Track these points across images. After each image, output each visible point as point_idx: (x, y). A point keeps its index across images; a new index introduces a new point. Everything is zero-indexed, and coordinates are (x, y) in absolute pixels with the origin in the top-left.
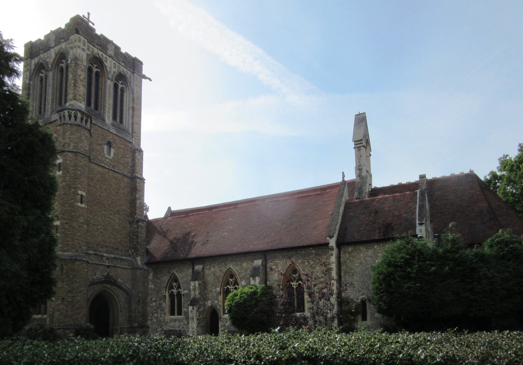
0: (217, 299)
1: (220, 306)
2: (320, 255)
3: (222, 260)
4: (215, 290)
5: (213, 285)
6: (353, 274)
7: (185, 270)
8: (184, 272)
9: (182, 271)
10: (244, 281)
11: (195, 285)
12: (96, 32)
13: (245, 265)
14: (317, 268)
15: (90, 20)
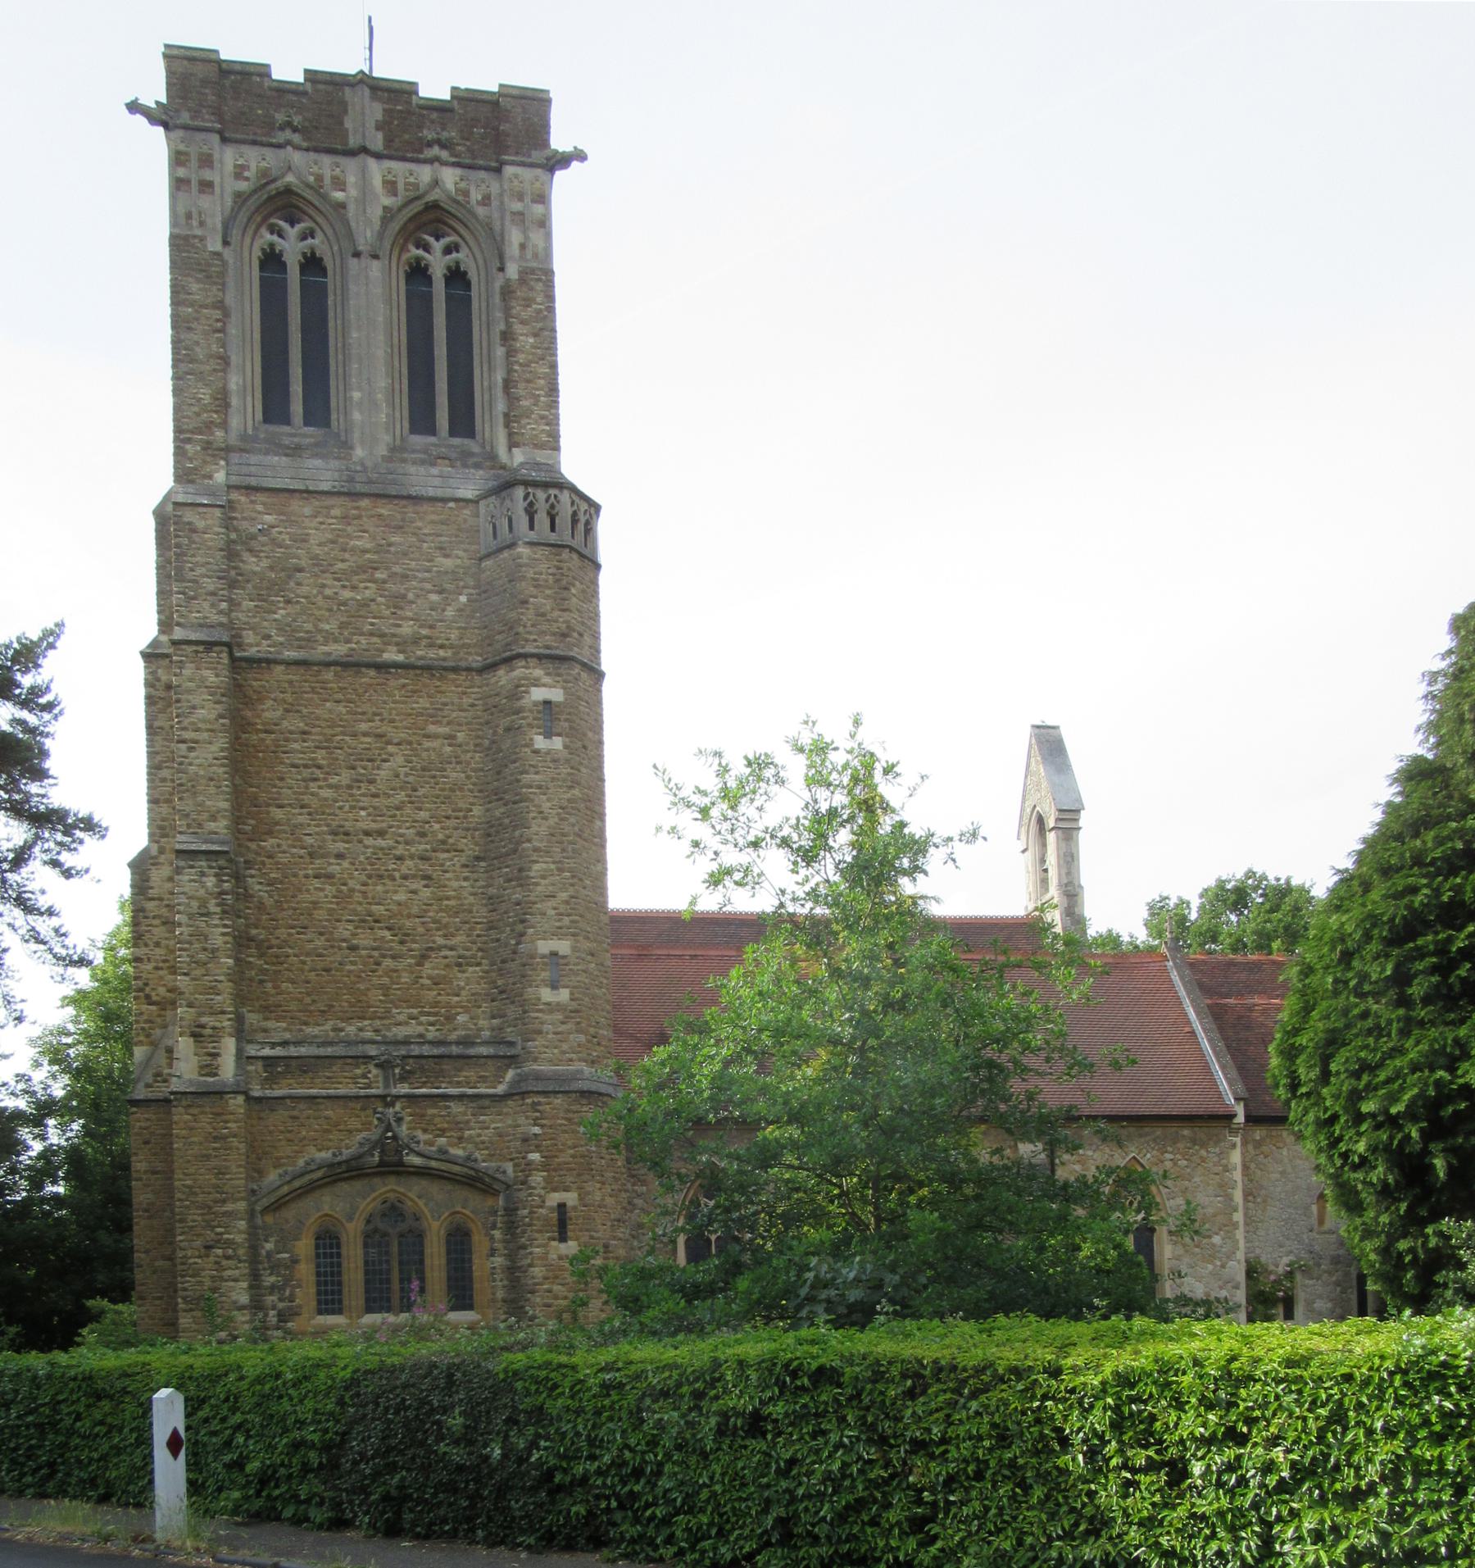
2: (1203, 1145)
6: (1265, 1201)
12: (422, 94)
14: (1197, 1179)
15: (161, 129)
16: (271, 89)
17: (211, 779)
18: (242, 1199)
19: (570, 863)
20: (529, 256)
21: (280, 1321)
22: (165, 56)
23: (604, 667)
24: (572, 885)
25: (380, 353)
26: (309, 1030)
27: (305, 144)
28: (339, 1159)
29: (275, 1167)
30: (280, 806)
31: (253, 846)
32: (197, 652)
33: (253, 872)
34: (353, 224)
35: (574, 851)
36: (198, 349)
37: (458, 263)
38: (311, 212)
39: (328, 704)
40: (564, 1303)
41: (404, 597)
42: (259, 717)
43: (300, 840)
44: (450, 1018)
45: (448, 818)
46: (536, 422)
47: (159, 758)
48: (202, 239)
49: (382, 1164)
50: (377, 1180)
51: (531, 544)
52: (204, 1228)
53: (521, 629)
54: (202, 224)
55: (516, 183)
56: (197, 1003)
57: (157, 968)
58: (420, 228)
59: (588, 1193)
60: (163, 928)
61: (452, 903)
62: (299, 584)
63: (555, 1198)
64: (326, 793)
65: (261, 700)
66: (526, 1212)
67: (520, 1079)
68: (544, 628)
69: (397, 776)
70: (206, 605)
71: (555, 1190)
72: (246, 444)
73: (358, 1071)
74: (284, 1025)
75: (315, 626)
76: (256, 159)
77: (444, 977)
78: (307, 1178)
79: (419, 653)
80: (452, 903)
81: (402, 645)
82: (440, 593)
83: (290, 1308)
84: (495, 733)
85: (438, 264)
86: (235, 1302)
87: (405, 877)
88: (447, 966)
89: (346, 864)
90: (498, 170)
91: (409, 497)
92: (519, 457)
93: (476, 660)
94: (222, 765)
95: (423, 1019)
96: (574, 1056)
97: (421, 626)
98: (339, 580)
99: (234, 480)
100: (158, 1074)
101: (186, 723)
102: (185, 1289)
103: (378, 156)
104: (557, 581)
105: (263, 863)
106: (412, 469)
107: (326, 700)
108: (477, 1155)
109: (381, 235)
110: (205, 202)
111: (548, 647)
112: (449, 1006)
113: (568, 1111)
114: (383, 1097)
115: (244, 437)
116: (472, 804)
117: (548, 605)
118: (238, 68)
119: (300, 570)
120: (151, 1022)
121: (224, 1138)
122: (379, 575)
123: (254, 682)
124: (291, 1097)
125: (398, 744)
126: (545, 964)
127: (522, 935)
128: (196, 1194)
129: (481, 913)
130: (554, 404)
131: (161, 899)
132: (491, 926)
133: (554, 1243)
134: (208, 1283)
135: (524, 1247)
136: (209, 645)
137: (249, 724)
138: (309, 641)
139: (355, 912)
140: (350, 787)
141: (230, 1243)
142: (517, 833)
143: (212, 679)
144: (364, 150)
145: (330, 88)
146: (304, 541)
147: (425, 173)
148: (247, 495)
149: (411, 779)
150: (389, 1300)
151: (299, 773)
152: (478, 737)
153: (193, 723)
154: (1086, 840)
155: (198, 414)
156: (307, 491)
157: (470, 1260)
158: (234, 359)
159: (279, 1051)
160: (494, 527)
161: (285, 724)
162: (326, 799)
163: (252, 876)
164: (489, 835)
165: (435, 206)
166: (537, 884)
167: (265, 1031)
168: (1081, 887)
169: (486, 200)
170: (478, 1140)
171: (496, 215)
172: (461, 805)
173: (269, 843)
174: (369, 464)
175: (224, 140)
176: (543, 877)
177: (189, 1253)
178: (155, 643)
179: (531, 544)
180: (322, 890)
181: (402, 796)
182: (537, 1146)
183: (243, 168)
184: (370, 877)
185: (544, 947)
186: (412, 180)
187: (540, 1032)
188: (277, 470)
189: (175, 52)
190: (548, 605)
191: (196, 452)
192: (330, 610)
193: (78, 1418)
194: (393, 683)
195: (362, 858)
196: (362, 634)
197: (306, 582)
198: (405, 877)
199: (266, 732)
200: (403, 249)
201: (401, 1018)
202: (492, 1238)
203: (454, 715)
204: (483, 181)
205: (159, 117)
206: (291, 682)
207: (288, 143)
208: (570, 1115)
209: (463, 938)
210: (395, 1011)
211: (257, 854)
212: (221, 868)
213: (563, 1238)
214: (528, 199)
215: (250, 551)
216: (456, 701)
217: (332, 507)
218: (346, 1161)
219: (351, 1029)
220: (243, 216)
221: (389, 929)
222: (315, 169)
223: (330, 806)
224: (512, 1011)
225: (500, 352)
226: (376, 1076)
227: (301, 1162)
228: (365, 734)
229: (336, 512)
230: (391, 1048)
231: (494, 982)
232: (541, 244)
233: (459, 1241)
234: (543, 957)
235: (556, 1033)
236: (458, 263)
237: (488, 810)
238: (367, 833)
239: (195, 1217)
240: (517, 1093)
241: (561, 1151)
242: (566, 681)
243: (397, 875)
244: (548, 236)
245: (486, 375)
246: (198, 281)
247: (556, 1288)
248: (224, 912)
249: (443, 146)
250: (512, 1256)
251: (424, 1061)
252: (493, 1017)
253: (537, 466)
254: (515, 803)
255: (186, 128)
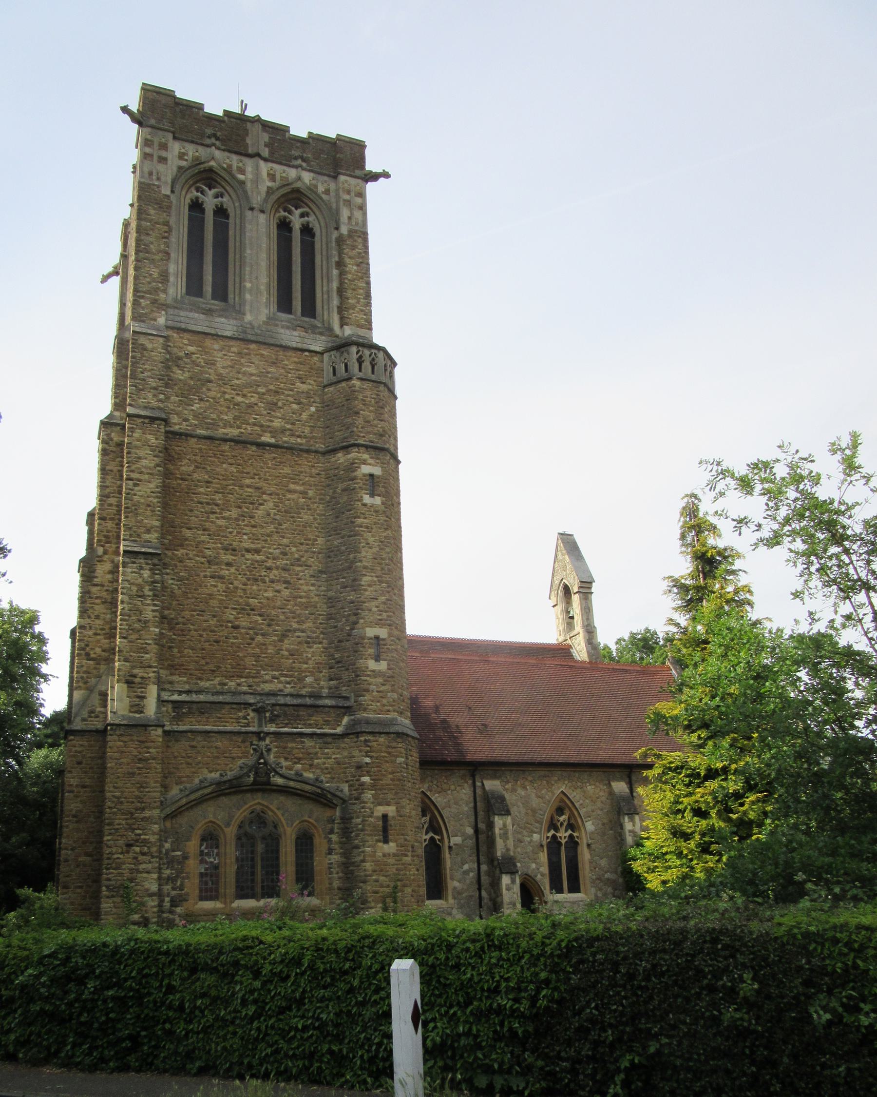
0: (535, 860)
1: (543, 875)
3: (542, 773)
4: (529, 839)
5: (525, 828)
7: (453, 787)
8: (449, 792)
9: (445, 791)
10: (590, 822)
11: (505, 825)
13: (590, 788)
16: (204, 116)
17: (149, 506)
18: (157, 807)
19: (387, 578)
20: (354, 223)
21: (172, 906)
22: (143, 89)
23: (400, 458)
24: (388, 592)
25: (264, 264)
26: (202, 684)
27: (223, 147)
28: (225, 778)
29: (177, 784)
30: (190, 529)
31: (169, 553)
32: (144, 423)
33: (168, 571)
34: (250, 193)
35: (389, 570)
36: (152, 246)
37: (308, 223)
38: (223, 183)
39: (224, 466)
40: (387, 890)
41: (276, 404)
42: (178, 469)
43: (202, 552)
44: (301, 679)
45: (302, 544)
46: (358, 312)
47: (108, 490)
48: (159, 187)
49: (255, 783)
50: (248, 795)
51: (362, 379)
52: (126, 830)
53: (355, 429)
54: (158, 179)
55: (346, 185)
56: (131, 659)
57: (96, 634)
58: (288, 201)
59: (403, 807)
60: (102, 606)
61: (304, 600)
62: (209, 390)
63: (380, 810)
64: (221, 522)
65: (180, 459)
66: (359, 820)
67: (354, 723)
68: (369, 429)
69: (269, 515)
70: (150, 395)
71: (380, 804)
72: (177, 305)
73: (240, 714)
74: (185, 679)
75: (218, 416)
76: (191, 151)
77: (297, 650)
78: (201, 792)
79: (285, 439)
80: (304, 600)
81: (274, 433)
82: (298, 404)
83: (180, 895)
84: (334, 492)
85: (297, 222)
86: (147, 890)
87: (272, 581)
88: (300, 643)
89: (233, 570)
90: (335, 177)
91: (281, 346)
92: (348, 331)
93: (321, 447)
94: (157, 497)
95: (282, 679)
96: (391, 708)
97: (287, 423)
98: (234, 390)
99: (170, 323)
100: (92, 712)
101: (133, 468)
102: (109, 880)
103: (266, 160)
104: (377, 403)
105: (176, 566)
106: (282, 331)
107: (223, 463)
108: (322, 778)
109: (266, 200)
110: (161, 167)
111: (372, 442)
112: (301, 671)
113: (389, 747)
114: (257, 734)
115: (175, 300)
116: (318, 536)
117: (372, 416)
118: (185, 102)
119: (210, 381)
120: (89, 673)
121: (146, 760)
122: (260, 390)
123: (177, 447)
124: (191, 731)
125: (271, 494)
126: (371, 644)
127: (356, 623)
128: (122, 803)
129: (323, 608)
130: (369, 304)
131: (102, 586)
132: (330, 617)
133: (380, 844)
134: (127, 874)
135: (357, 847)
136: (153, 419)
137: (172, 474)
138: (214, 425)
139: (237, 602)
140: (237, 519)
141: (145, 842)
142: (351, 556)
143: (152, 439)
144: (258, 155)
145: (239, 122)
146: (212, 364)
147: (292, 173)
148: (178, 333)
149: (278, 517)
150: (253, 888)
151: (203, 508)
152: (321, 494)
153: (139, 468)
154: (595, 599)
155: (149, 283)
156: (217, 335)
157: (312, 857)
158: (173, 255)
159: (184, 697)
160: (334, 369)
161: (195, 475)
162: (221, 526)
163: (167, 574)
164: (329, 557)
165: (297, 191)
166: (366, 590)
167: (171, 683)
168: (595, 627)
169: (327, 192)
170: (323, 766)
171: (333, 200)
172: (310, 536)
173: (180, 552)
174: (256, 325)
175: (175, 138)
176: (370, 586)
177: (114, 850)
178: (110, 416)
179: (362, 379)
180: (215, 586)
181: (271, 528)
182: (368, 772)
183: (184, 154)
184: (248, 579)
185: (371, 632)
186: (284, 175)
187: (367, 690)
188: (198, 321)
189: (149, 88)
190: (372, 416)
191: (147, 305)
192: (229, 408)
193: (171, 989)
194: (267, 455)
195: (244, 567)
196: (248, 424)
197: (213, 389)
198: (272, 581)
199: (182, 479)
200: (277, 211)
201: (267, 677)
202: (330, 841)
203: (307, 479)
204: (326, 182)
205: (134, 118)
206: (200, 449)
207: (214, 145)
208: (390, 750)
209: (311, 624)
210: (262, 672)
211: (172, 559)
212: (154, 565)
213: (386, 841)
214: (353, 194)
215: (178, 366)
216: (308, 470)
217: (232, 346)
218: (229, 780)
219: (232, 684)
220: (183, 180)
221: (260, 615)
222: (228, 161)
223: (223, 531)
224: (345, 676)
225: (335, 272)
226: (252, 718)
227: (197, 781)
228: (248, 486)
229: (234, 349)
230: (264, 698)
231: (333, 655)
232: (360, 219)
233: (305, 842)
234: (370, 639)
235: (378, 692)
236: (308, 223)
237: (328, 541)
238: (248, 551)
239: (120, 821)
240: (352, 733)
241: (384, 775)
242: (382, 463)
243: (267, 579)
244: (365, 214)
245: (325, 284)
246: (154, 209)
247: (382, 878)
248: (155, 595)
249: (304, 160)
250: (347, 854)
251: (286, 709)
252: (331, 679)
253: (363, 337)
254: (350, 536)
255: (152, 127)
